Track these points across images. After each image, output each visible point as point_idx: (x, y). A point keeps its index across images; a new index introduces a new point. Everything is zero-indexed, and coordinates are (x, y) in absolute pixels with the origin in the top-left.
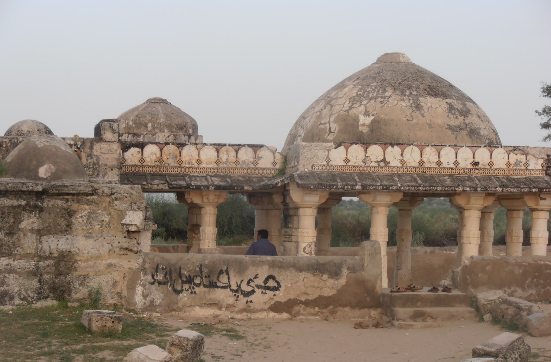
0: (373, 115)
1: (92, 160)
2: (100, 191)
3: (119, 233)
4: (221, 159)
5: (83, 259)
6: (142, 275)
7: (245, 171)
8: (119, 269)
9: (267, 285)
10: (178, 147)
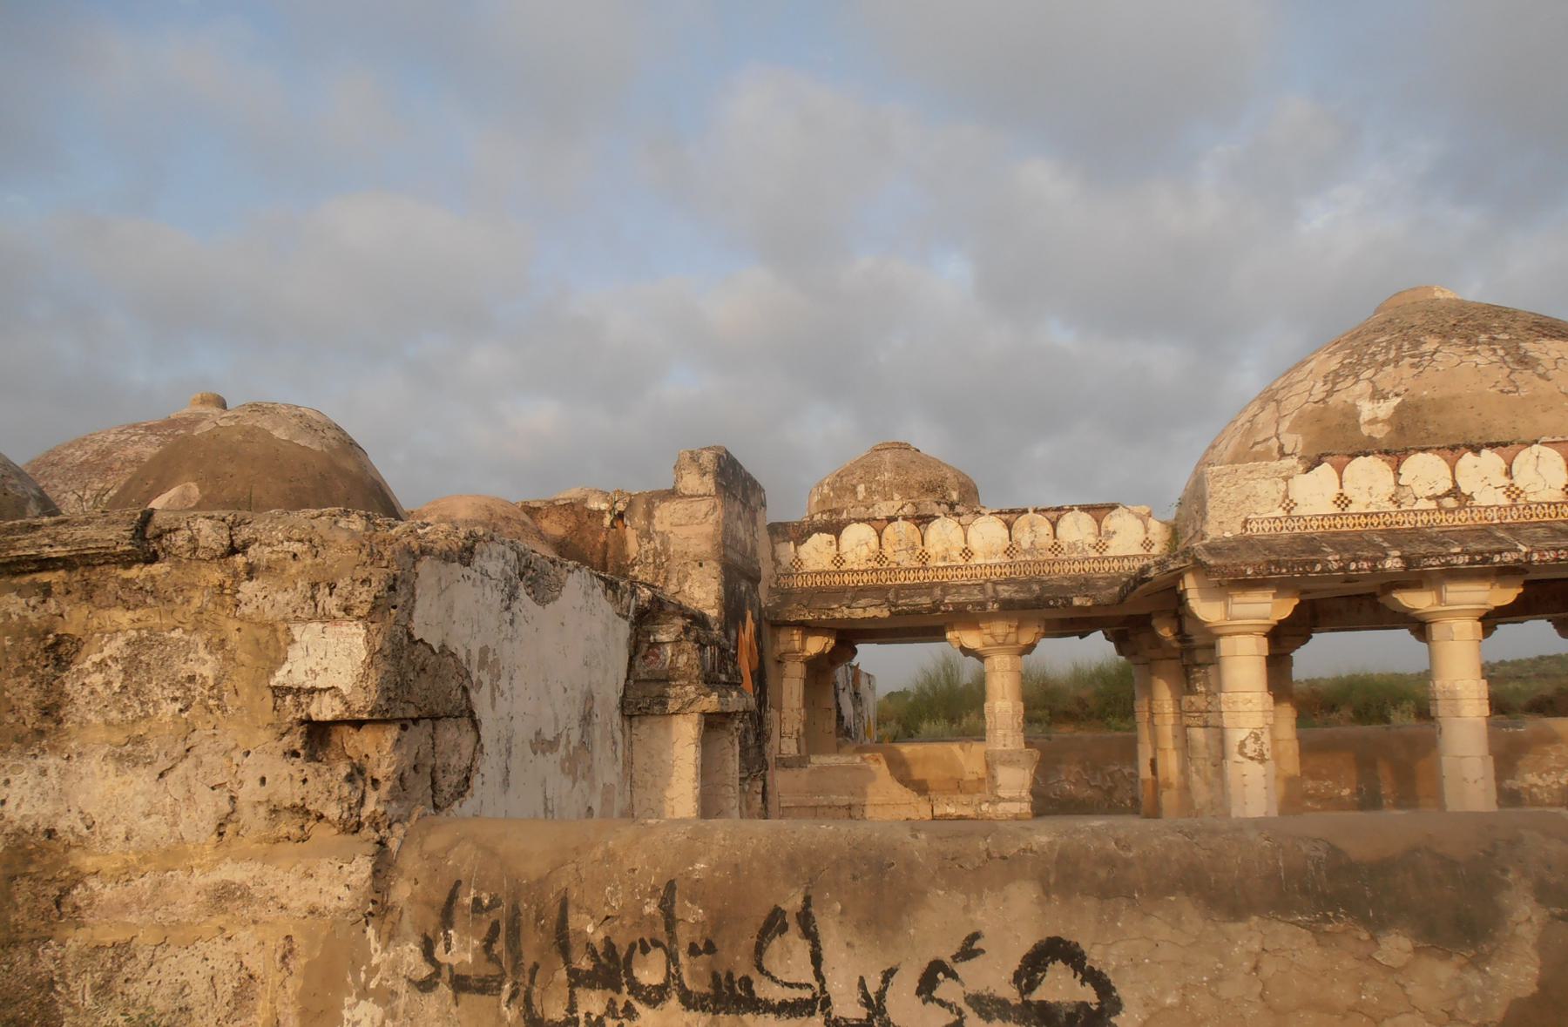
0: (1397, 395)
1: (652, 544)
2: (180, 539)
3: (265, 736)
4: (1018, 543)
5: (108, 866)
6: (374, 944)
7: (1077, 567)
8: (263, 915)
9: (1035, 996)
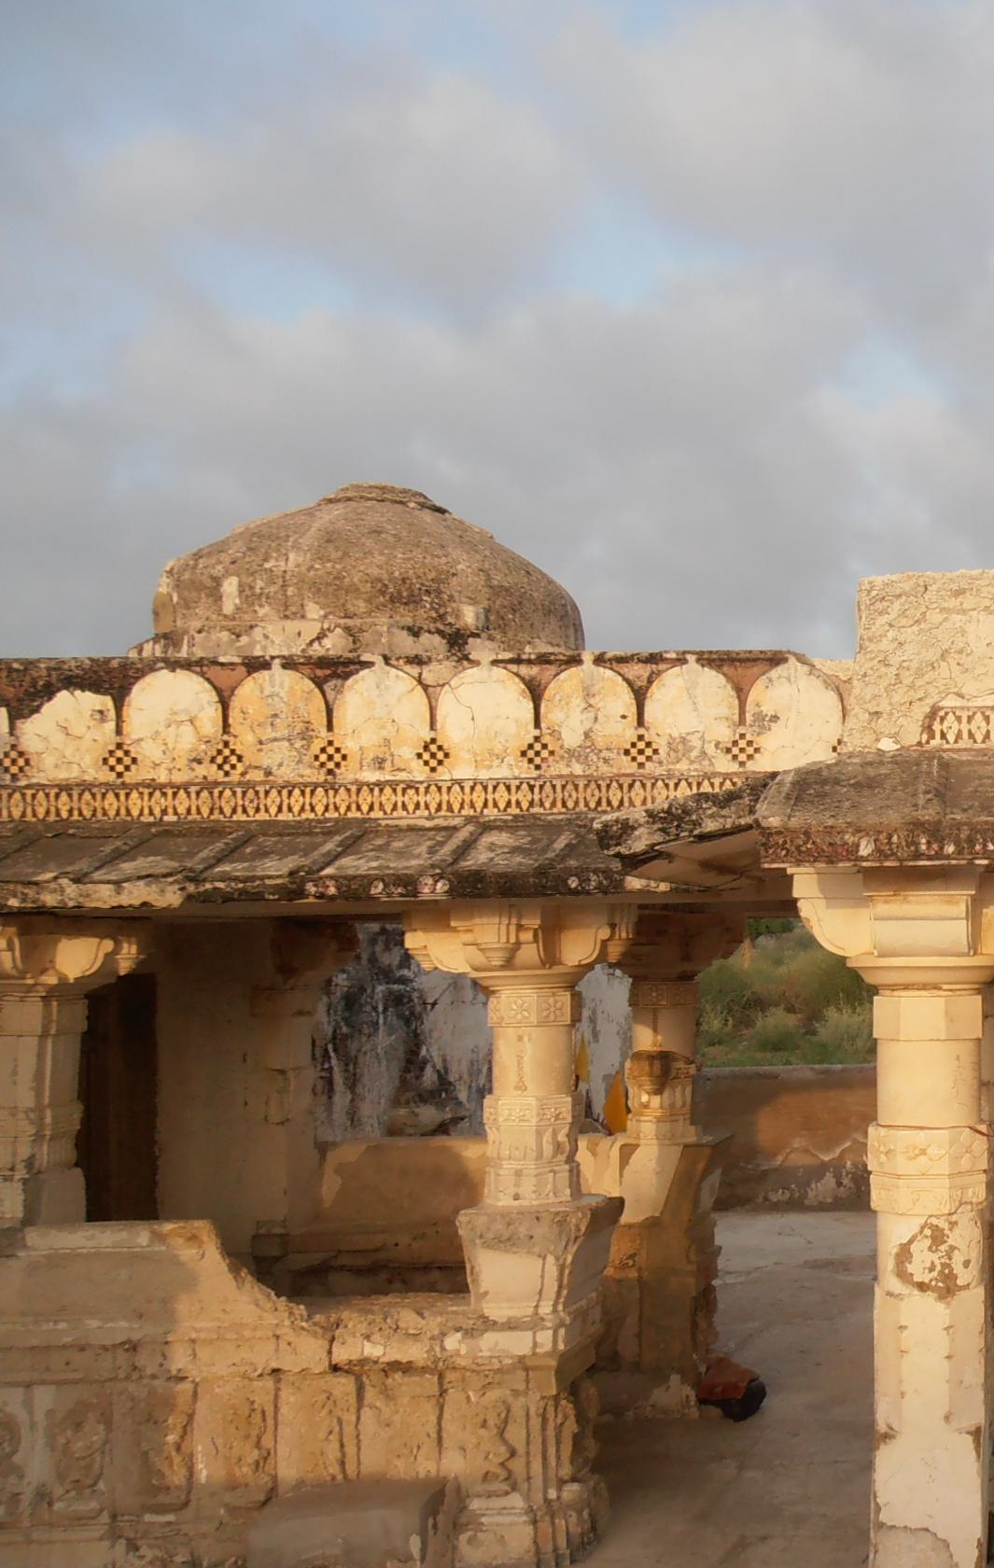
4: (555, 734)
10: (319, 683)
